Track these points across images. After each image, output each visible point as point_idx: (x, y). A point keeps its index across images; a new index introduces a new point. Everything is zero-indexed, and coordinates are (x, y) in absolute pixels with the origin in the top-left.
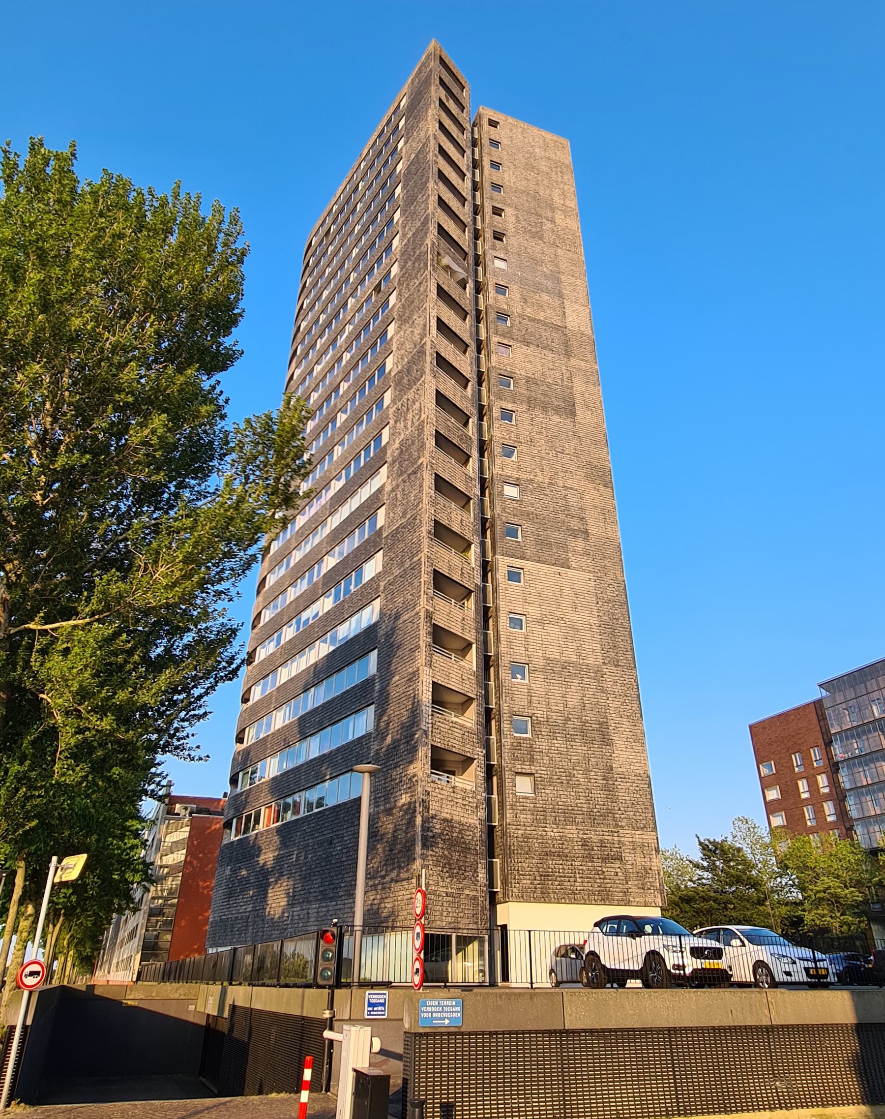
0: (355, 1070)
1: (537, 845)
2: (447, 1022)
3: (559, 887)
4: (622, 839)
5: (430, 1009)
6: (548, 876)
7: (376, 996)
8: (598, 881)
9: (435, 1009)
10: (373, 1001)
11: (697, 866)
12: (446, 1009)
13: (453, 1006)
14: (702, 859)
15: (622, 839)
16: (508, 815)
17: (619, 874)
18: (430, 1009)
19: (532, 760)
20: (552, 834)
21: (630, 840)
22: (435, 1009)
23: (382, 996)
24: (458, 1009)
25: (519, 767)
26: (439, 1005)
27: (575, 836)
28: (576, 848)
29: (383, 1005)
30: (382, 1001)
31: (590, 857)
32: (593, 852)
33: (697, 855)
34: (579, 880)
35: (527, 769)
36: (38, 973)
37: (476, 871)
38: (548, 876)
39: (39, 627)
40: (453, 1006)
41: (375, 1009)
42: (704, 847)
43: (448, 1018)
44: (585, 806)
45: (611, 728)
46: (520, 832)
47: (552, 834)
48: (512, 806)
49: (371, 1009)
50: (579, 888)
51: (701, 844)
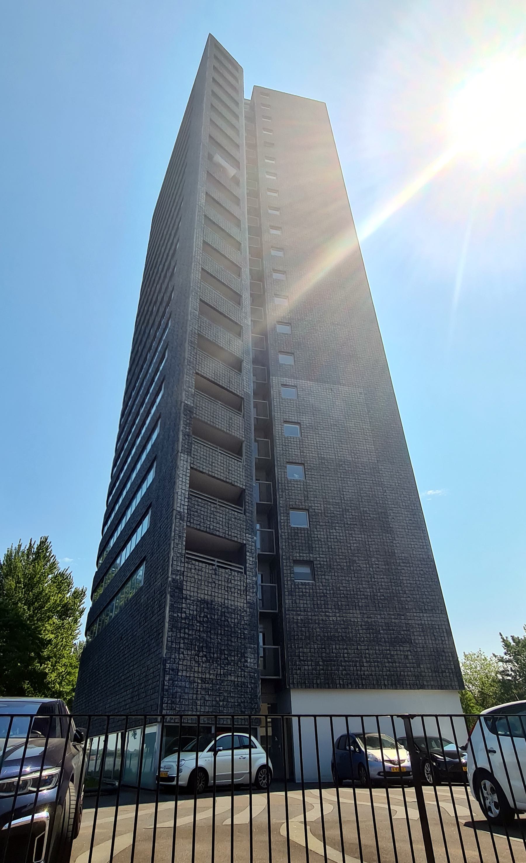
0: (213, 46)
1: (318, 630)
3: (344, 672)
4: (410, 622)
6: (331, 661)
8: (387, 664)
11: (501, 660)
14: (505, 654)
15: (410, 622)
16: (287, 601)
17: (410, 657)
19: (310, 549)
20: (334, 618)
21: (419, 622)
25: (297, 556)
28: (361, 631)
33: (501, 651)
34: (365, 664)
35: (305, 556)
36: (267, 172)
37: (243, 655)
38: (331, 661)
39: (247, 235)
42: (507, 645)
44: (368, 590)
45: (390, 517)
47: (334, 618)
48: (291, 594)
50: (366, 673)
51: (504, 641)
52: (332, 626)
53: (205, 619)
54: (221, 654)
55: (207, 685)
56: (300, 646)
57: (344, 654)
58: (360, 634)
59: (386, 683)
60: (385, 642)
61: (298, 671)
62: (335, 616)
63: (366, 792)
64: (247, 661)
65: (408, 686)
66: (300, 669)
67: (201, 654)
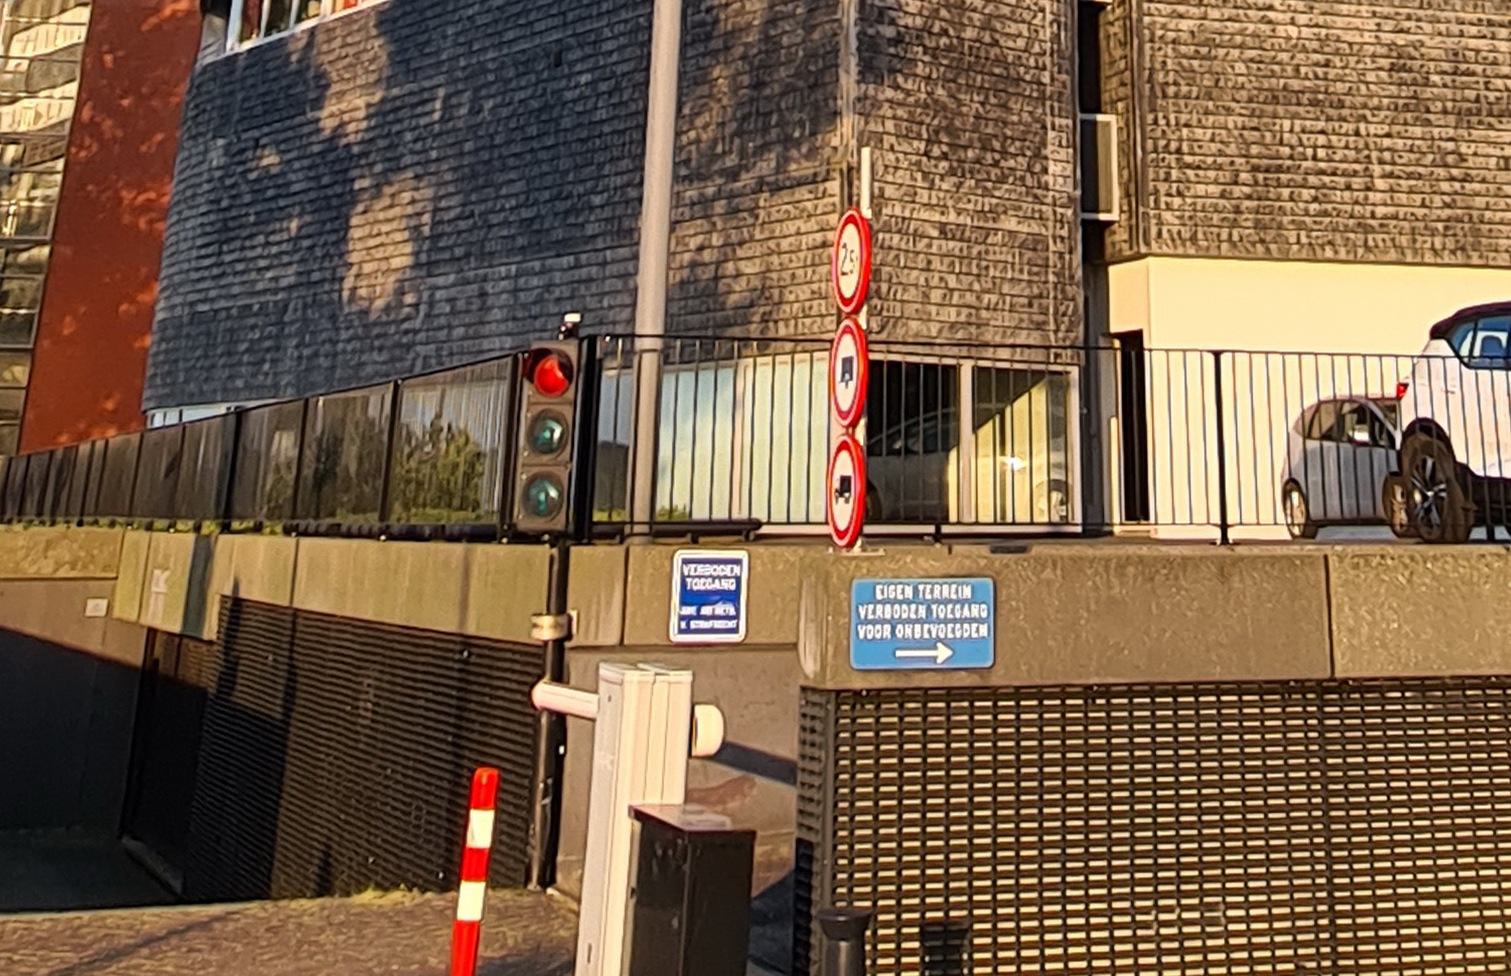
1: (1240, 68)
2: (943, 653)
5: (886, 611)
6: (1279, 169)
7: (709, 569)
8: (1445, 186)
9: (903, 611)
10: (698, 585)
12: (940, 611)
13: (962, 602)
18: (886, 611)
20: (1293, 31)
22: (903, 611)
23: (727, 569)
24: (981, 610)
26: (916, 600)
27: (1368, 37)
28: (1371, 77)
29: (732, 597)
30: (729, 585)
31: (1417, 108)
32: (1428, 93)
34: (1380, 184)
37: (1038, 155)
38: (1279, 169)
40: (962, 602)
41: (706, 610)
43: (946, 642)
46: (1185, 25)
49: (690, 610)
50: (1380, 211)
52: (1284, 57)
53: (944, 41)
54: (984, 148)
55: (951, 244)
56: (1184, 118)
57: (1315, 147)
58: (1367, 83)
59: (1438, 246)
60: (1445, 112)
61: (1177, 201)
62: (1293, 22)
63: (1487, 373)
64: (1045, 171)
65: (632, 193)
66: (1180, 194)
67: (936, 151)
